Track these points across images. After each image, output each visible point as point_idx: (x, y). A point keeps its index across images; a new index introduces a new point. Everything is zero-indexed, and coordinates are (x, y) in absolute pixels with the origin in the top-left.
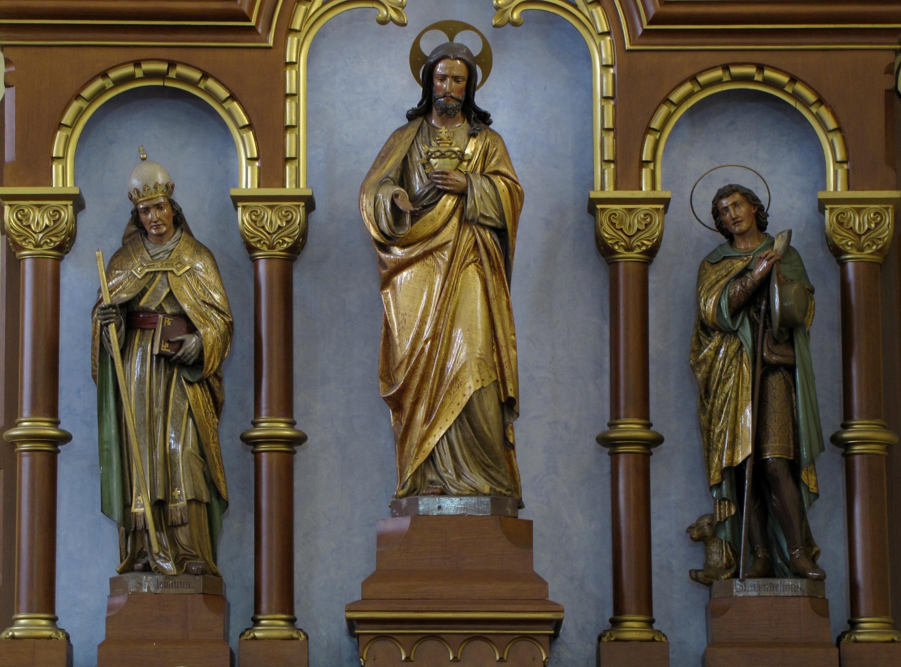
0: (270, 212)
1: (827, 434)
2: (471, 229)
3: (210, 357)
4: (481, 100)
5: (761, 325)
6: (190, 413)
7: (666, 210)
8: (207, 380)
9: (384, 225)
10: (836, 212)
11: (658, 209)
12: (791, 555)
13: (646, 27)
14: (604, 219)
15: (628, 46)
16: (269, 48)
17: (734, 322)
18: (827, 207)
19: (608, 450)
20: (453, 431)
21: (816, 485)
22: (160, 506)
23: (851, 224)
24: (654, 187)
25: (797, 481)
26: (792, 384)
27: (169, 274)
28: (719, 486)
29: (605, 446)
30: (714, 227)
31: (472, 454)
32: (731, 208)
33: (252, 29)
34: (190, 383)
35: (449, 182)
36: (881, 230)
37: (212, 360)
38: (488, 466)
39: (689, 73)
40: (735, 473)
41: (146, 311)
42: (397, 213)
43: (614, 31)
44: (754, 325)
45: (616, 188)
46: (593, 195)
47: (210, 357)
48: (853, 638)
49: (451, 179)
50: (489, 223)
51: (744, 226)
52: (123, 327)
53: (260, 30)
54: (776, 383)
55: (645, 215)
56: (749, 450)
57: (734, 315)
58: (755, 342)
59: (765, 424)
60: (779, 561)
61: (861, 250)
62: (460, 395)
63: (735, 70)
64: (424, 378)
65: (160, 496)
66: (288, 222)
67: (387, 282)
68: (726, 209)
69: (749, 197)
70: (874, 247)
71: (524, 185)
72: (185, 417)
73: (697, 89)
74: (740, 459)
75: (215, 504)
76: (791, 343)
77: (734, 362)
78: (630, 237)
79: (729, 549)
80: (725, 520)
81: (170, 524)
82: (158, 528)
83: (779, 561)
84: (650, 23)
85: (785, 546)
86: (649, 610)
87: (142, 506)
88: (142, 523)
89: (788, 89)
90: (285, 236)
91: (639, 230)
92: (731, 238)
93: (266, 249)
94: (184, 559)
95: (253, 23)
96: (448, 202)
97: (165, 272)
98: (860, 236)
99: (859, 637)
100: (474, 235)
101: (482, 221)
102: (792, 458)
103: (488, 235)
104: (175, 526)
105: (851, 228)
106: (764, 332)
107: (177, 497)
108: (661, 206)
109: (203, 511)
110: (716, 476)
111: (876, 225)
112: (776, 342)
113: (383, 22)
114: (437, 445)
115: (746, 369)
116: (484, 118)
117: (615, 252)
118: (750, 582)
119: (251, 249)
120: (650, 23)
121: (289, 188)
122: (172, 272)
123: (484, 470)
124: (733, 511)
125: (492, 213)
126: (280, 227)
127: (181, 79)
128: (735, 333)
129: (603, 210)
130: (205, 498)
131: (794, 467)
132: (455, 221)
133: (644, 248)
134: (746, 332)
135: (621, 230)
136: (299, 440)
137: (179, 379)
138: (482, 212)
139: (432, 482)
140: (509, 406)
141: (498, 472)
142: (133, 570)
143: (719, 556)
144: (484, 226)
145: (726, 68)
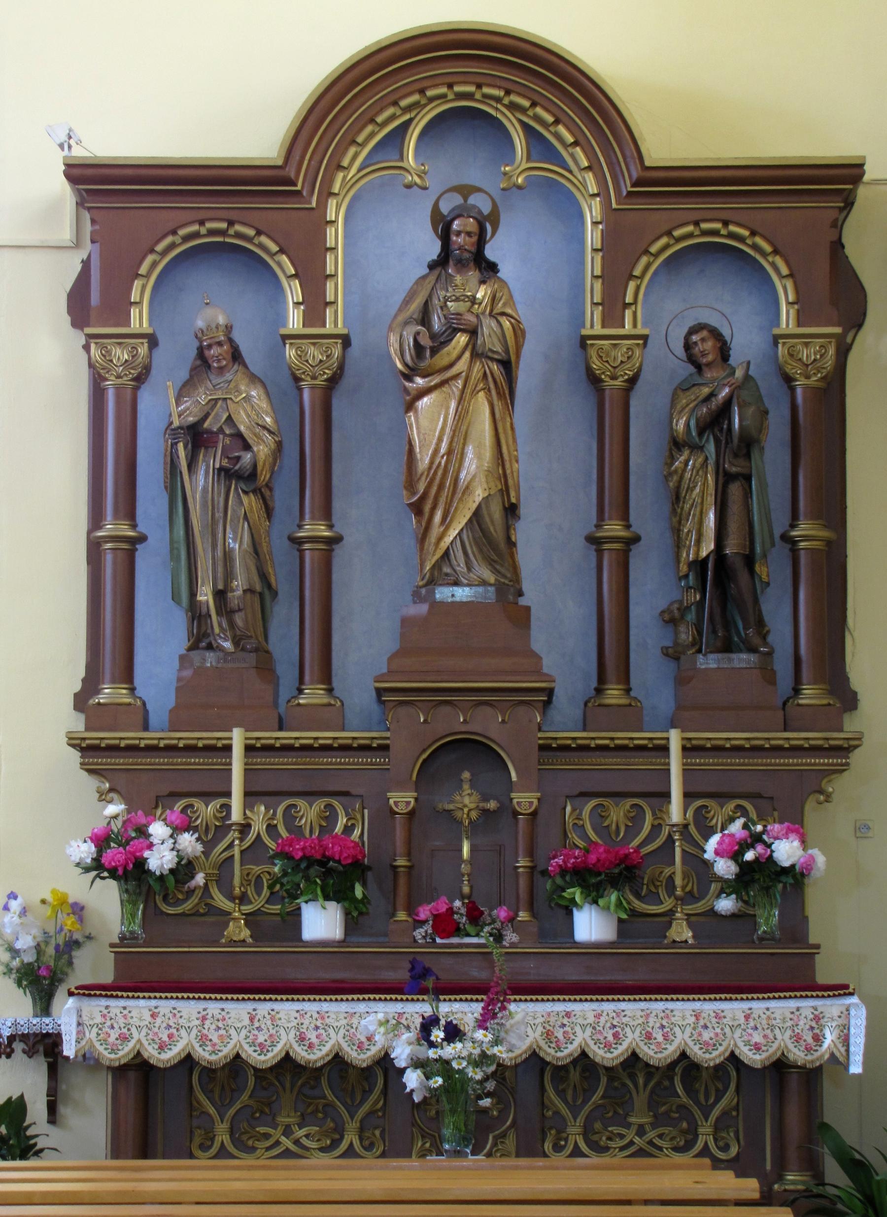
0: (312, 348)
3: (262, 470)
4: (491, 252)
5: (724, 442)
6: (246, 517)
7: (645, 345)
8: (260, 490)
9: (408, 358)
10: (787, 346)
11: (638, 345)
12: (746, 634)
13: (630, 189)
14: (593, 353)
15: (614, 206)
16: (312, 209)
19: (594, 547)
20: (465, 531)
21: (768, 576)
22: (220, 595)
23: (800, 356)
24: (635, 325)
27: (229, 401)
28: (686, 576)
29: (592, 544)
31: (481, 551)
32: (699, 343)
33: (298, 193)
35: (463, 322)
36: (824, 361)
38: (495, 561)
40: (700, 565)
41: (209, 431)
42: (419, 348)
43: (602, 193)
44: (717, 442)
45: (603, 326)
46: (584, 332)
47: (262, 470)
48: (796, 702)
49: (464, 320)
50: (496, 356)
51: (710, 358)
52: (190, 446)
54: (735, 490)
55: (628, 349)
57: (701, 434)
59: (726, 524)
60: (736, 639)
61: (808, 377)
62: (471, 501)
65: (220, 587)
67: (410, 406)
69: (716, 334)
71: (525, 325)
72: (241, 521)
73: (672, 242)
74: (704, 553)
75: (267, 592)
76: (748, 456)
78: (615, 368)
79: (694, 629)
81: (228, 610)
82: (218, 613)
83: (736, 639)
84: (633, 186)
85: (741, 626)
87: (205, 595)
88: (206, 609)
89: (749, 241)
90: (327, 368)
91: (622, 362)
92: (699, 368)
93: (309, 380)
94: (240, 639)
95: (299, 188)
96: (462, 339)
98: (807, 366)
99: (801, 702)
100: (483, 366)
102: (747, 553)
104: (233, 612)
106: (726, 447)
107: (234, 587)
108: (641, 342)
109: (257, 599)
110: (684, 568)
112: (736, 455)
113: (409, 186)
117: (602, 381)
118: (711, 656)
119: (297, 379)
120: (633, 186)
121: (329, 328)
122: (231, 399)
123: (490, 564)
124: (698, 597)
125: (498, 348)
127: (238, 235)
128: (701, 448)
129: (592, 345)
130: (258, 587)
131: (749, 560)
132: (467, 355)
133: (626, 377)
134: (711, 447)
135: (607, 362)
136: (337, 540)
137: (236, 489)
138: (490, 346)
139: (447, 575)
140: (511, 511)
141: (502, 566)
143: (686, 635)
144: (492, 359)
145: (697, 223)
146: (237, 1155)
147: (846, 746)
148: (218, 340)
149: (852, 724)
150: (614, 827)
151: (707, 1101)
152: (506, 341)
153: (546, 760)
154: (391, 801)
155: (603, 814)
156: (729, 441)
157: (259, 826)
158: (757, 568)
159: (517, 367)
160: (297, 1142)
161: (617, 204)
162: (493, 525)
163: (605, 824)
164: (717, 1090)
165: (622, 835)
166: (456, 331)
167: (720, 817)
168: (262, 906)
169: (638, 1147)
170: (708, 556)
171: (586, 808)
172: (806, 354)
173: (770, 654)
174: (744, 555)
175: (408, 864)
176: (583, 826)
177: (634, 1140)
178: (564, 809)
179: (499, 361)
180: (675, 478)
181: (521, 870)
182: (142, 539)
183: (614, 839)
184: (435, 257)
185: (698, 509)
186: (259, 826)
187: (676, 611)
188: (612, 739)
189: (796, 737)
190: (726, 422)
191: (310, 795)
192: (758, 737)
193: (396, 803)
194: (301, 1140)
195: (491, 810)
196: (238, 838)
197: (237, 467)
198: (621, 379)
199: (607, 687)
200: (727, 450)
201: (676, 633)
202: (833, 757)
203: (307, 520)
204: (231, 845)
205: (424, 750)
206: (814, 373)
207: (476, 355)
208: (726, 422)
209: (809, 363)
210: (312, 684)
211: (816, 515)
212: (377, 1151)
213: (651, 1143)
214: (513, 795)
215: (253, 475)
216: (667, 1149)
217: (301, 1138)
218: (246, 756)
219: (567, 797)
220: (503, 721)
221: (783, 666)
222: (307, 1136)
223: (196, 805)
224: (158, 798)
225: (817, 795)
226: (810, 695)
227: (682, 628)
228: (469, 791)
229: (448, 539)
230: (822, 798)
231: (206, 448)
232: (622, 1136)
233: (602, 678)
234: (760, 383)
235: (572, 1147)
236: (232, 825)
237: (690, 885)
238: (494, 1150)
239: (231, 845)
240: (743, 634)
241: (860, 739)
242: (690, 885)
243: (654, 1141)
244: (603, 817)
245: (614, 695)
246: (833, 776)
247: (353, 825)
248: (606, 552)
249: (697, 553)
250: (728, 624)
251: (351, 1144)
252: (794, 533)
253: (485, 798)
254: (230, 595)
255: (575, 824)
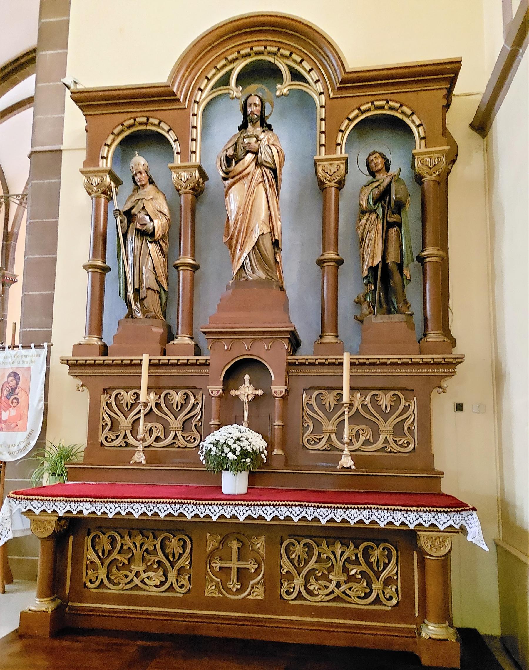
0: (184, 173)
1: (415, 255)
2: (261, 168)
5: (386, 208)
6: (149, 253)
9: (224, 168)
10: (420, 160)
12: (398, 306)
14: (319, 169)
16: (185, 108)
17: (375, 207)
18: (416, 157)
20: (251, 253)
21: (410, 276)
22: (137, 291)
23: (427, 164)
25: (402, 274)
26: (400, 232)
27: (144, 200)
28: (367, 277)
30: (369, 175)
31: (260, 264)
32: (374, 160)
34: (151, 242)
35: (251, 147)
37: (159, 232)
38: (268, 270)
39: (356, 106)
40: (373, 270)
44: (383, 207)
48: (426, 340)
50: (268, 165)
51: (380, 167)
53: (181, 101)
54: (393, 232)
55: (337, 165)
56: (380, 259)
57: (375, 204)
58: (383, 215)
59: (388, 248)
60: (393, 310)
61: (431, 175)
63: (377, 103)
64: (239, 232)
65: (137, 286)
66: (191, 177)
68: (372, 160)
69: (384, 157)
70: (437, 172)
71: (284, 151)
74: (375, 264)
75: (162, 292)
76: (400, 214)
77: (374, 223)
78: (331, 176)
80: (370, 292)
82: (135, 301)
83: (393, 310)
84: (340, 84)
85: (395, 304)
86: (336, 331)
87: (130, 293)
91: (334, 172)
97: (142, 199)
98: (431, 168)
99: (428, 340)
100: (262, 170)
101: (265, 164)
102: (399, 263)
103: (268, 171)
105: (427, 165)
106: (388, 209)
110: (365, 273)
111: (438, 163)
112: (393, 213)
114: (245, 260)
115: (380, 226)
116: (270, 127)
117: (324, 183)
118: (379, 316)
119: (178, 190)
120: (340, 84)
121: (338, 155)
122: (145, 199)
123: (266, 272)
125: (269, 160)
126: (188, 179)
128: (375, 211)
129: (319, 165)
131: (400, 267)
132: (253, 164)
133: (336, 180)
134: (380, 211)
135: (327, 173)
138: (265, 159)
141: (272, 273)
142: (128, 318)
143: (366, 309)
144: (267, 167)
146: (109, 587)
147: (454, 362)
148: (139, 170)
149: (457, 351)
150: (327, 405)
151: (378, 569)
152: (274, 158)
153: (293, 371)
154: (210, 391)
155: (322, 398)
156: (390, 206)
157: (357, 405)
158: (404, 271)
159: (281, 173)
160: (142, 581)
161: (333, 94)
162: (266, 250)
163: (323, 403)
164: (384, 563)
165: (332, 409)
166: (248, 152)
167: (385, 400)
168: (360, 447)
169: (337, 595)
170: (378, 264)
171: (314, 394)
172: (430, 162)
173: (411, 315)
174: (397, 263)
175: (218, 423)
176: (312, 404)
177: (334, 590)
178: (302, 395)
179: (270, 168)
180: (361, 228)
181: (276, 427)
182: (109, 269)
183: (328, 411)
184: (241, 123)
185: (373, 241)
186: (357, 405)
187: (362, 297)
188: (327, 359)
189: (427, 357)
190: (388, 197)
191: (176, 389)
192: (405, 358)
193: (212, 392)
194: (144, 580)
195: (259, 395)
196: (143, 409)
197: (144, 229)
198: (334, 181)
199: (325, 334)
200: (389, 211)
201: (362, 310)
202: (447, 369)
203: (181, 256)
204: (139, 412)
205: (227, 364)
206: (434, 172)
207: (258, 164)
208: (388, 197)
209: (432, 166)
210: (182, 333)
211: (436, 245)
212: (185, 589)
213: (344, 592)
214: (272, 387)
215: (152, 235)
216: (354, 597)
217: (145, 578)
218: (149, 369)
219: (304, 389)
220: (268, 349)
221: (418, 319)
222: (148, 578)
223: (122, 393)
224: (105, 389)
225: (438, 389)
226: (433, 337)
227: (364, 306)
228: (248, 385)
229: (243, 259)
230: (441, 390)
231: (133, 222)
232: (327, 587)
233: (323, 330)
234: (404, 179)
235: (297, 592)
236: (343, 404)
237: (369, 436)
238: (252, 592)
239: (139, 412)
240: (396, 307)
241: (462, 358)
242: (369, 436)
243: (346, 591)
244: (322, 400)
245: (329, 338)
246: (446, 379)
247: (197, 403)
248: (326, 267)
249: (373, 263)
250: (389, 302)
251: (172, 584)
252: (424, 253)
253: (256, 389)
254: (141, 291)
255: (307, 403)
